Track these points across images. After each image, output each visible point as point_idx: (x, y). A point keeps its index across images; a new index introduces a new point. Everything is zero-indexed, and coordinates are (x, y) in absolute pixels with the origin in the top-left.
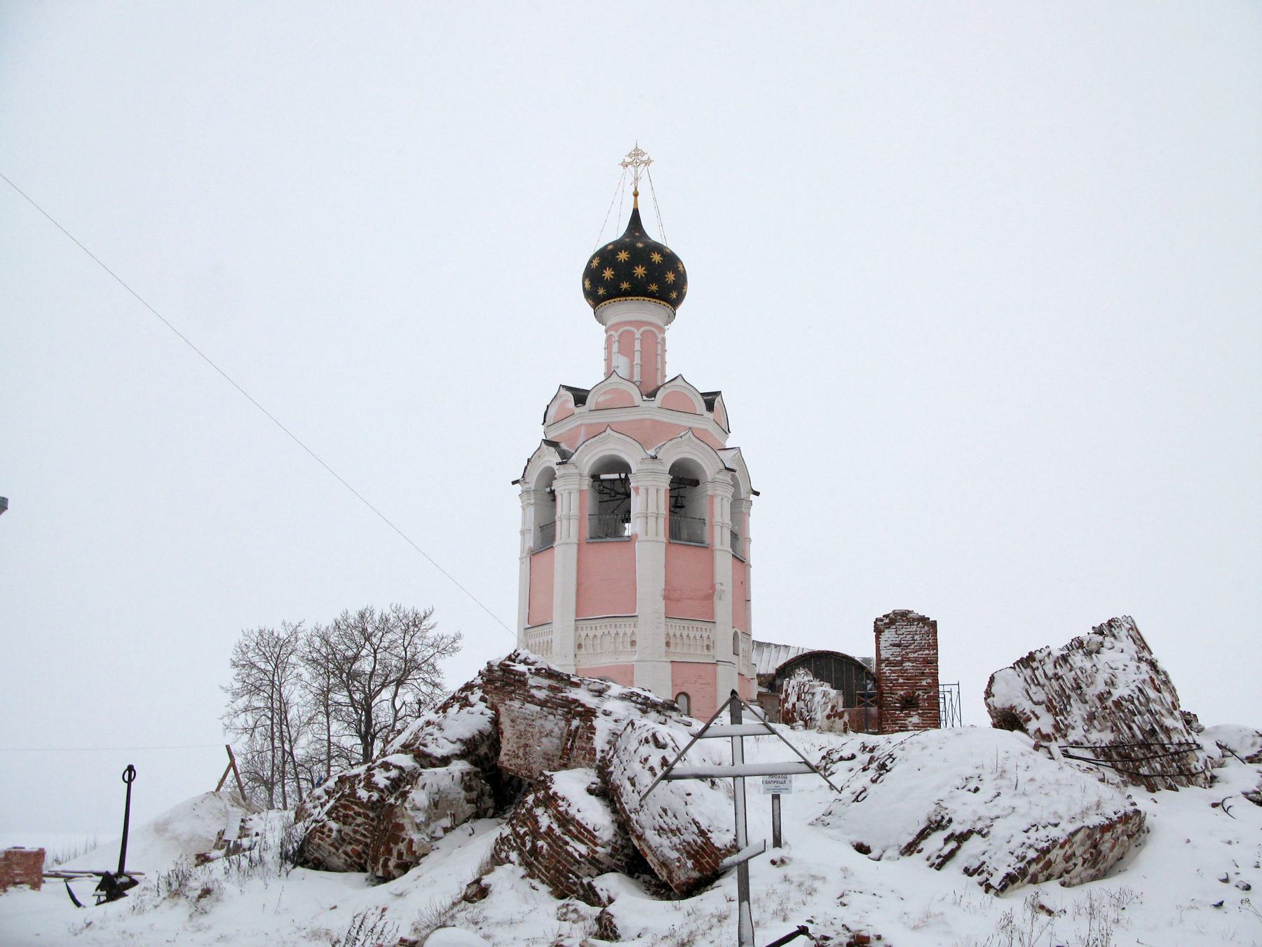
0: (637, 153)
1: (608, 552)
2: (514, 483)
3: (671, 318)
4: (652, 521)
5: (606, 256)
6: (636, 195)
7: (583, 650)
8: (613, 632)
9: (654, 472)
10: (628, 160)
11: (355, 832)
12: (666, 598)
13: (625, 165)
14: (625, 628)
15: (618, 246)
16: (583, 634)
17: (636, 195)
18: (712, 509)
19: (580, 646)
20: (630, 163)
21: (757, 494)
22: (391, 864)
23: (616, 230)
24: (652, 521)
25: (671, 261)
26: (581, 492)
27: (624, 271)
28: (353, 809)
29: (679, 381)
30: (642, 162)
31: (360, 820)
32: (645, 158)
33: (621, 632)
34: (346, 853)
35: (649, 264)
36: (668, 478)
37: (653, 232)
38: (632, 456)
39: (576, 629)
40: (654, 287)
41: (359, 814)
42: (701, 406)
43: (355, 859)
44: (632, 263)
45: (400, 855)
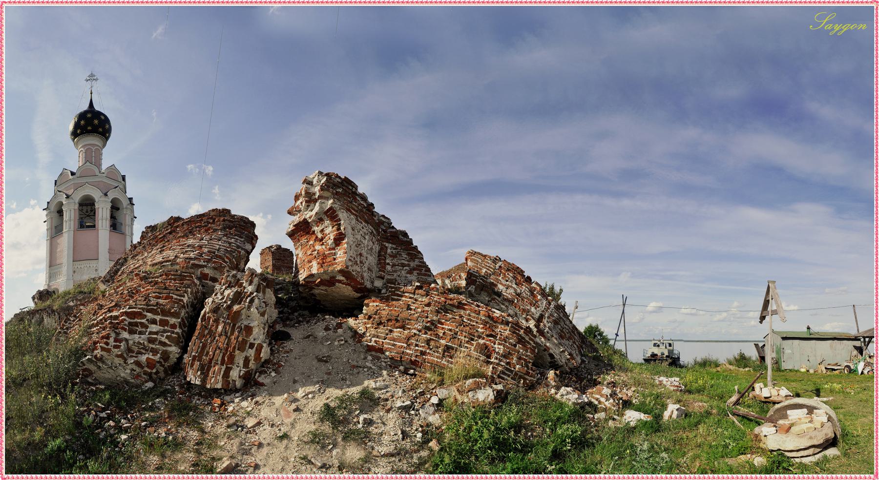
0: (92, 75)
1: (87, 234)
2: (44, 210)
3: (104, 146)
4: (104, 221)
5: (82, 116)
6: (91, 93)
7: (76, 273)
8: (88, 266)
9: (106, 201)
10: (88, 78)
11: (151, 341)
12: (109, 252)
13: (87, 80)
14: (93, 264)
15: (86, 112)
16: (76, 267)
17: (91, 93)
18: (125, 220)
19: (74, 272)
20: (89, 80)
21: (136, 218)
22: (235, 374)
23: (85, 107)
24: (104, 221)
25: (107, 120)
26: (74, 209)
27: (89, 122)
28: (146, 316)
29: (113, 167)
30: (94, 79)
31: (154, 328)
32: (95, 78)
33: (91, 266)
34: (138, 363)
35: (99, 119)
36: (110, 205)
37: (97, 108)
38: (96, 195)
39: (73, 265)
40: (101, 130)
41: (154, 322)
42: (120, 179)
43: (146, 369)
44: (92, 118)
45: (247, 361)
